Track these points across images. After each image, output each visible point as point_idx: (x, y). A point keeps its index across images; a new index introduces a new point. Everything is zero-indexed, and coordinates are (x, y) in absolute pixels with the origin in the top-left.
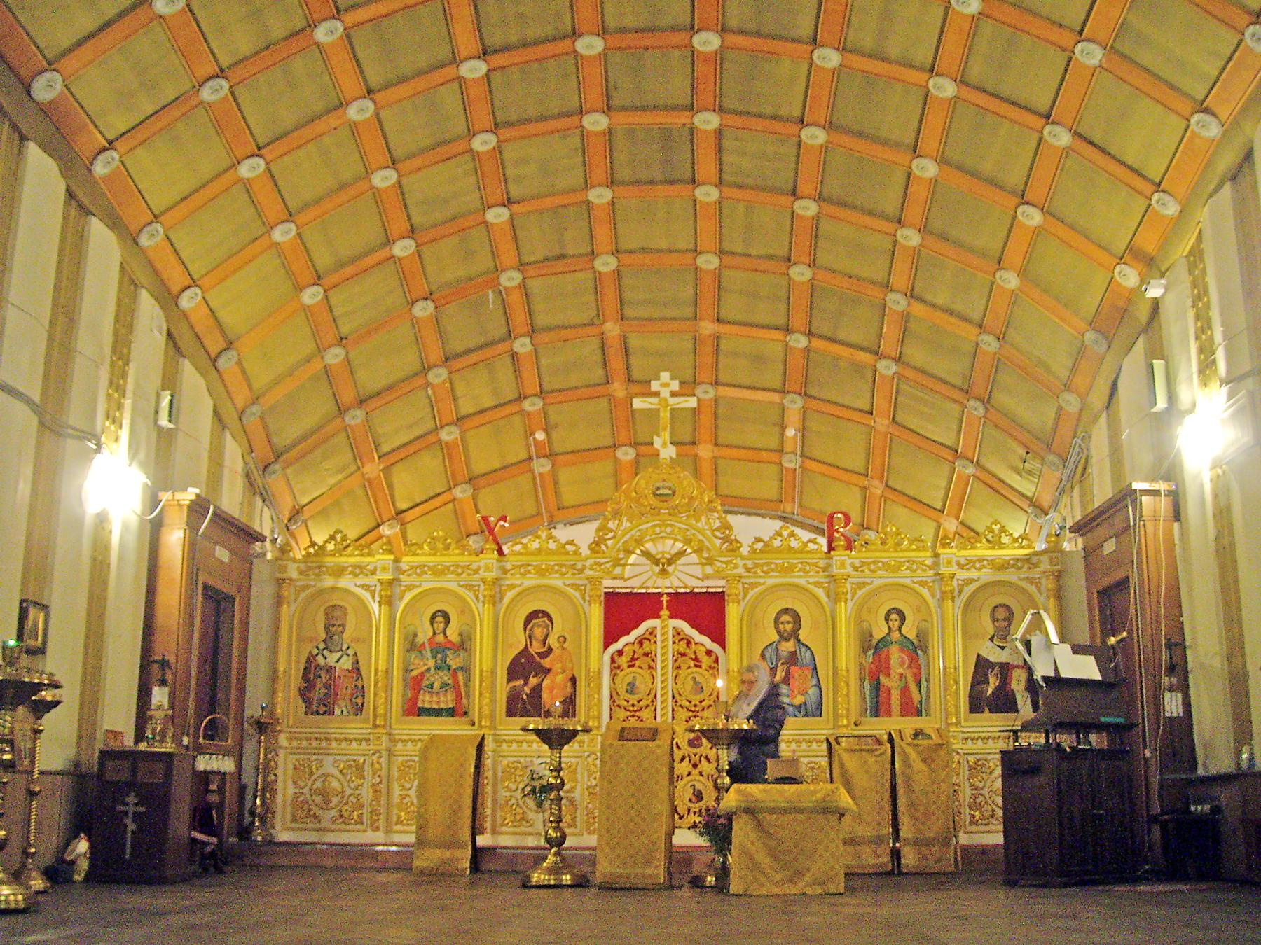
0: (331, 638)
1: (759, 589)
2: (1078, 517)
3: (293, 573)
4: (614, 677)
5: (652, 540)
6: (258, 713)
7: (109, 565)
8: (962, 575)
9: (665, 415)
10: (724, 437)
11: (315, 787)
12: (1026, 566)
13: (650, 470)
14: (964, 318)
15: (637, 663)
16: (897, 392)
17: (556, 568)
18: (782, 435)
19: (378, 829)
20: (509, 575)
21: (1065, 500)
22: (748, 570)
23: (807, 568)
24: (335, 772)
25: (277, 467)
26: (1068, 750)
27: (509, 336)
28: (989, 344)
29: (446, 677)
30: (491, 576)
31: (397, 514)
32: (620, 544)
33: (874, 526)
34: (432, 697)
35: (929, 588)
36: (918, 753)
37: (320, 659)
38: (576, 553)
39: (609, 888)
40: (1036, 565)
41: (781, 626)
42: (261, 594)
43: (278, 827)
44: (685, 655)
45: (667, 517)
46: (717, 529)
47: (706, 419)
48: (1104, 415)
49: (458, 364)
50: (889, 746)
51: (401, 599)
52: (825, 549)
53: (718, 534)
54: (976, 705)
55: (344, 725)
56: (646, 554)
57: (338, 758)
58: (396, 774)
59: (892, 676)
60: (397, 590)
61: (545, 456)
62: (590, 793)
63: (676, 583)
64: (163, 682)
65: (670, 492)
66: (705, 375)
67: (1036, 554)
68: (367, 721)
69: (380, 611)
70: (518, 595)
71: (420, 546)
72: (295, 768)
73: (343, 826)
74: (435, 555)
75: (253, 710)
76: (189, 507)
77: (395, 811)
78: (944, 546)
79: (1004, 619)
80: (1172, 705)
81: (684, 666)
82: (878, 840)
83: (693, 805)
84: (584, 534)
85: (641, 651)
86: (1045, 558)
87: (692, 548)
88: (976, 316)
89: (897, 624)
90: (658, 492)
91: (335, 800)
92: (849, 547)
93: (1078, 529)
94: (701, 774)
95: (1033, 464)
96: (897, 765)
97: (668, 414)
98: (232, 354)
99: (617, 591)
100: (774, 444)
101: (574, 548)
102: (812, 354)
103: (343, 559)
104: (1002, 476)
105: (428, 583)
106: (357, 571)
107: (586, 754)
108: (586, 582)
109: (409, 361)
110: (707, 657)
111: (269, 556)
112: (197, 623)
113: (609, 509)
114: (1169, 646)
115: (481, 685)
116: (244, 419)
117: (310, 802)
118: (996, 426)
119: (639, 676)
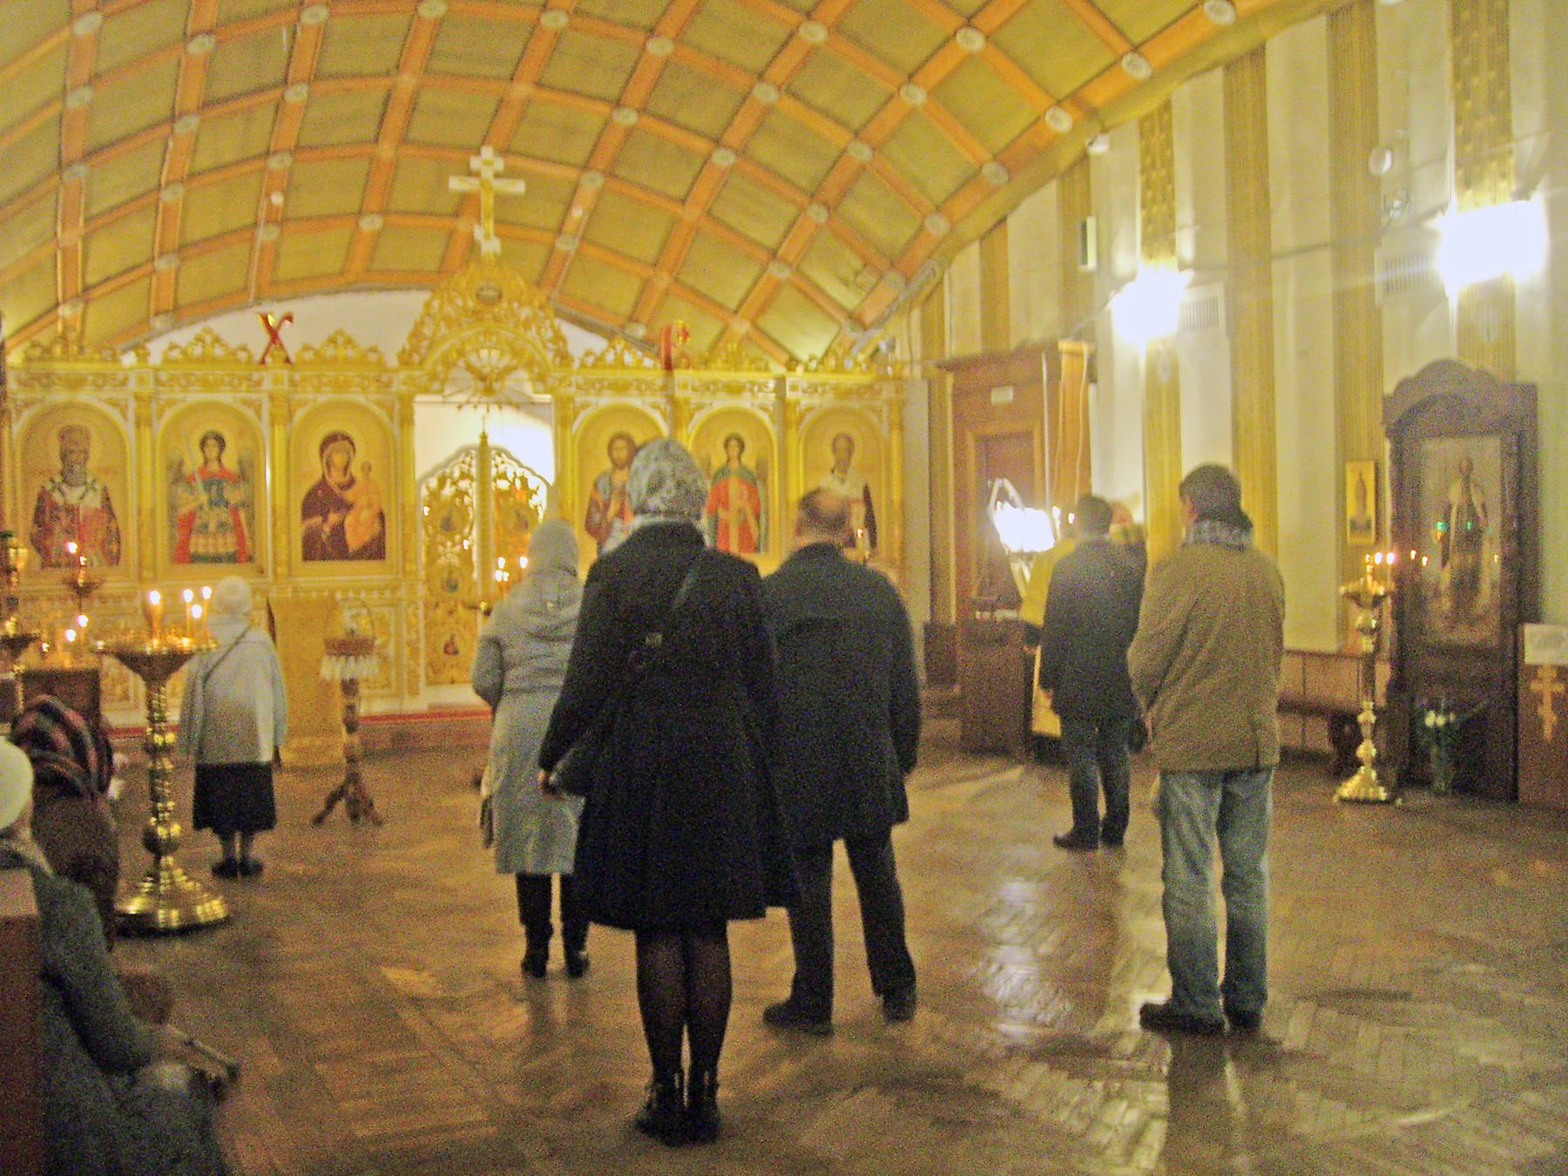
1: (591, 411)
9: (488, 202)
14: (837, 121)
37: (57, 497)
51: (160, 416)
56: (469, 368)
69: (139, 439)
95: (868, 279)
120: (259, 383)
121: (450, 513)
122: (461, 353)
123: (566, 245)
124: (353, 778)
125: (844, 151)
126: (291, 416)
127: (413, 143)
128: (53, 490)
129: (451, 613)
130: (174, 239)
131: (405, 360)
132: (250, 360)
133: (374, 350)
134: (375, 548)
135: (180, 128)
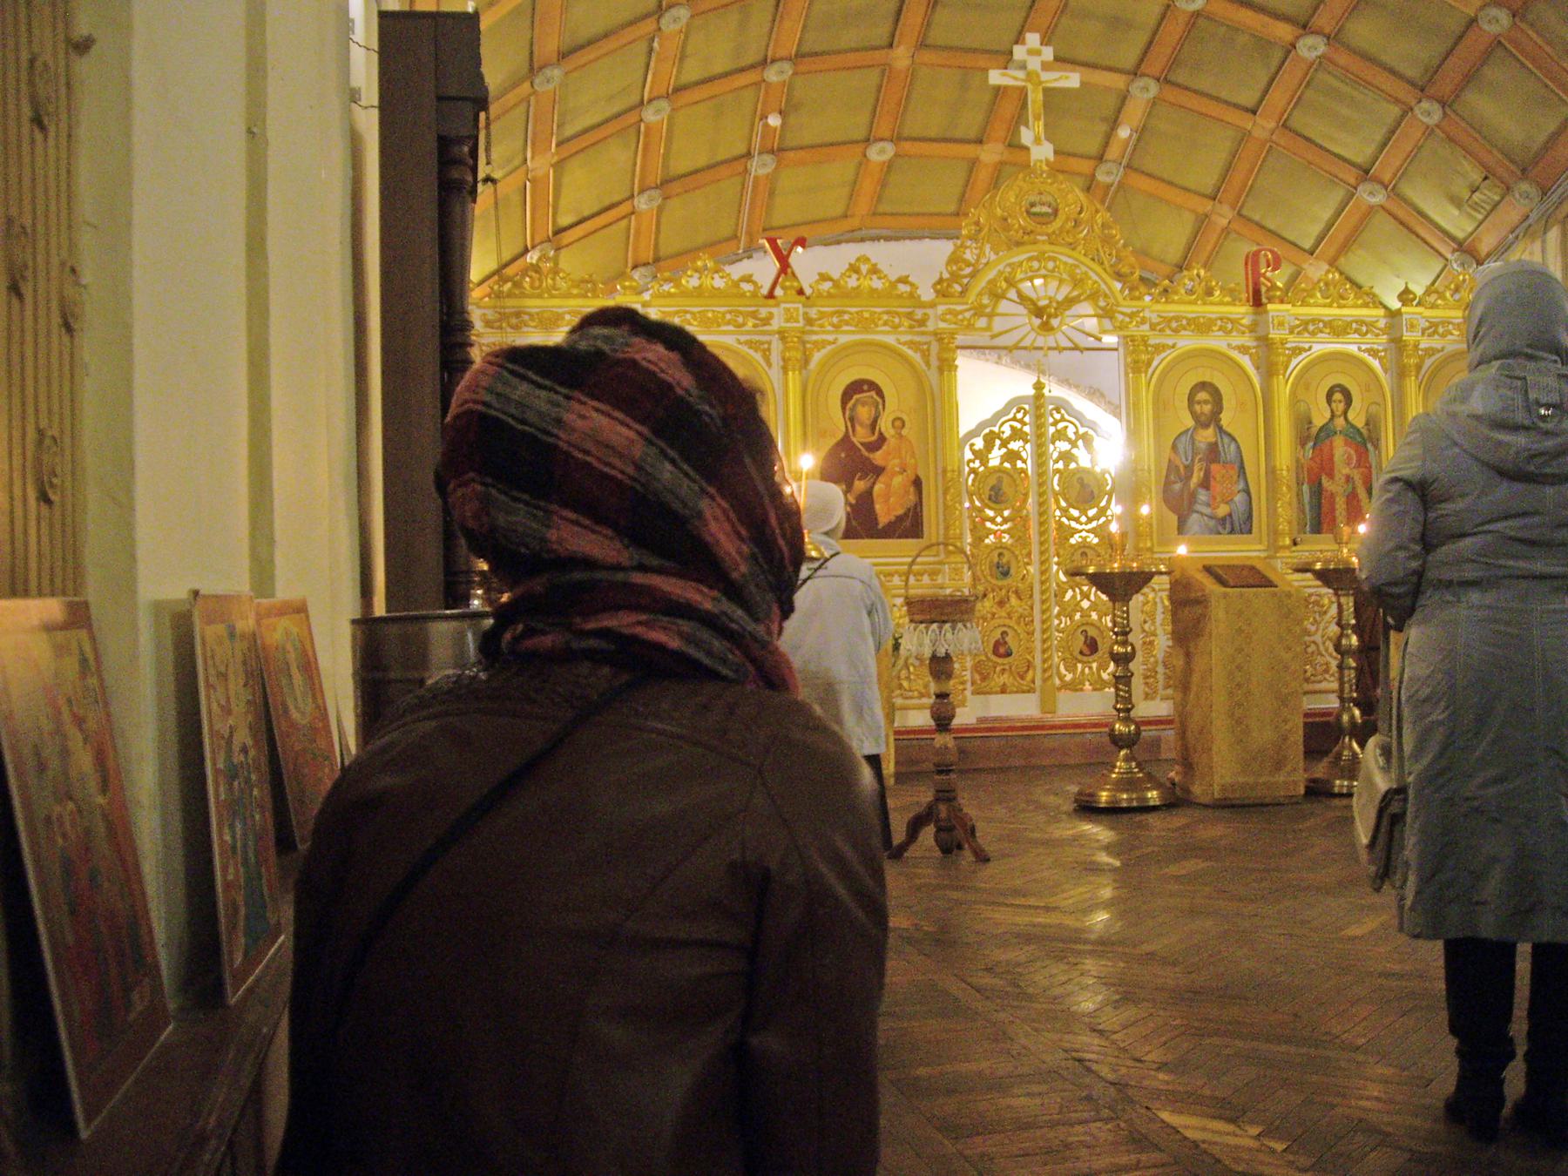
1: (1169, 356)
5: (1044, 277)
9: (1035, 98)
17: (728, 316)
35: (1381, 359)
41: (1197, 408)
45: (1047, 247)
56: (1023, 299)
59: (1337, 478)
61: (772, 152)
65: (1050, 210)
89: (1341, 407)
90: (1034, 210)
95: (1489, 194)
97: (1040, 96)
101: (908, 288)
120: (767, 321)
121: (1000, 480)
122: (1011, 282)
124: (946, 795)
125: (1473, 21)
126: (806, 361)
127: (935, 47)
129: (1001, 603)
130: (656, 176)
131: (942, 289)
132: (754, 295)
133: (904, 280)
134: (907, 523)
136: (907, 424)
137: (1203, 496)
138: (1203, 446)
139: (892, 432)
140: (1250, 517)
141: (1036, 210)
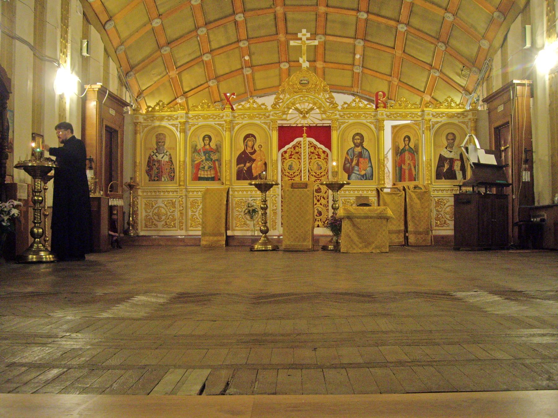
0: (159, 147)
2: (485, 96)
3: (141, 119)
4: (283, 163)
5: (299, 103)
6: (129, 181)
7: (66, 118)
8: (434, 120)
9: (304, 48)
10: (328, 58)
11: (154, 212)
12: (462, 116)
13: (298, 72)
15: (293, 157)
16: (406, 39)
18: (354, 57)
19: (182, 229)
20: (236, 119)
21: (480, 88)
22: (341, 116)
23: (367, 116)
24: (163, 205)
25: (132, 73)
26: (483, 194)
27: (234, 13)
28: (450, 17)
29: (210, 164)
30: (229, 119)
31: (184, 93)
32: (285, 105)
33: (393, 98)
34: (204, 172)
36: (416, 195)
38: (265, 109)
39: (287, 250)
40: (466, 116)
41: (355, 141)
42: (128, 129)
43: (139, 230)
44: (314, 153)
45: (306, 93)
46: (328, 99)
47: (321, 51)
48: (500, 50)
49: (211, 26)
50: (404, 192)
52: (374, 107)
53: (328, 100)
54: (439, 176)
55: (166, 186)
56: (296, 109)
57: (164, 199)
58: (189, 206)
60: (188, 126)
61: (249, 67)
62: (274, 213)
63: (310, 122)
64: (91, 168)
66: (320, 31)
67: (466, 111)
68: (176, 183)
70: (240, 128)
71: (197, 107)
72: (146, 204)
73: (167, 229)
74: (203, 110)
75: (127, 179)
76: (98, 91)
77: (190, 222)
78: (426, 107)
79: (452, 139)
80: (526, 176)
81: (313, 158)
82: (399, 232)
83: (317, 217)
84: (269, 101)
85: (294, 152)
86: (470, 113)
87: (316, 106)
88: (444, 5)
90: (302, 82)
91: (163, 217)
92: (385, 107)
93: (485, 101)
94: (321, 204)
96: (407, 200)
97: (305, 48)
98: (111, 23)
99: (284, 125)
100: (350, 61)
102: (369, 22)
103: (163, 113)
104: (451, 77)
105: (202, 122)
106: (170, 118)
107: (272, 196)
108: (270, 121)
109: (189, 24)
110: (323, 154)
111: (130, 113)
112: (104, 143)
113: (280, 90)
114: (526, 151)
115: (226, 166)
116: (117, 52)
117: (153, 218)
118: (451, 55)
119: (294, 162)
123: (357, 70)
128: (153, 155)
135: (199, 32)
136: (263, 147)
137: (356, 168)
138: (357, 153)
139: (258, 149)
140: (372, 175)
141: (303, 82)
